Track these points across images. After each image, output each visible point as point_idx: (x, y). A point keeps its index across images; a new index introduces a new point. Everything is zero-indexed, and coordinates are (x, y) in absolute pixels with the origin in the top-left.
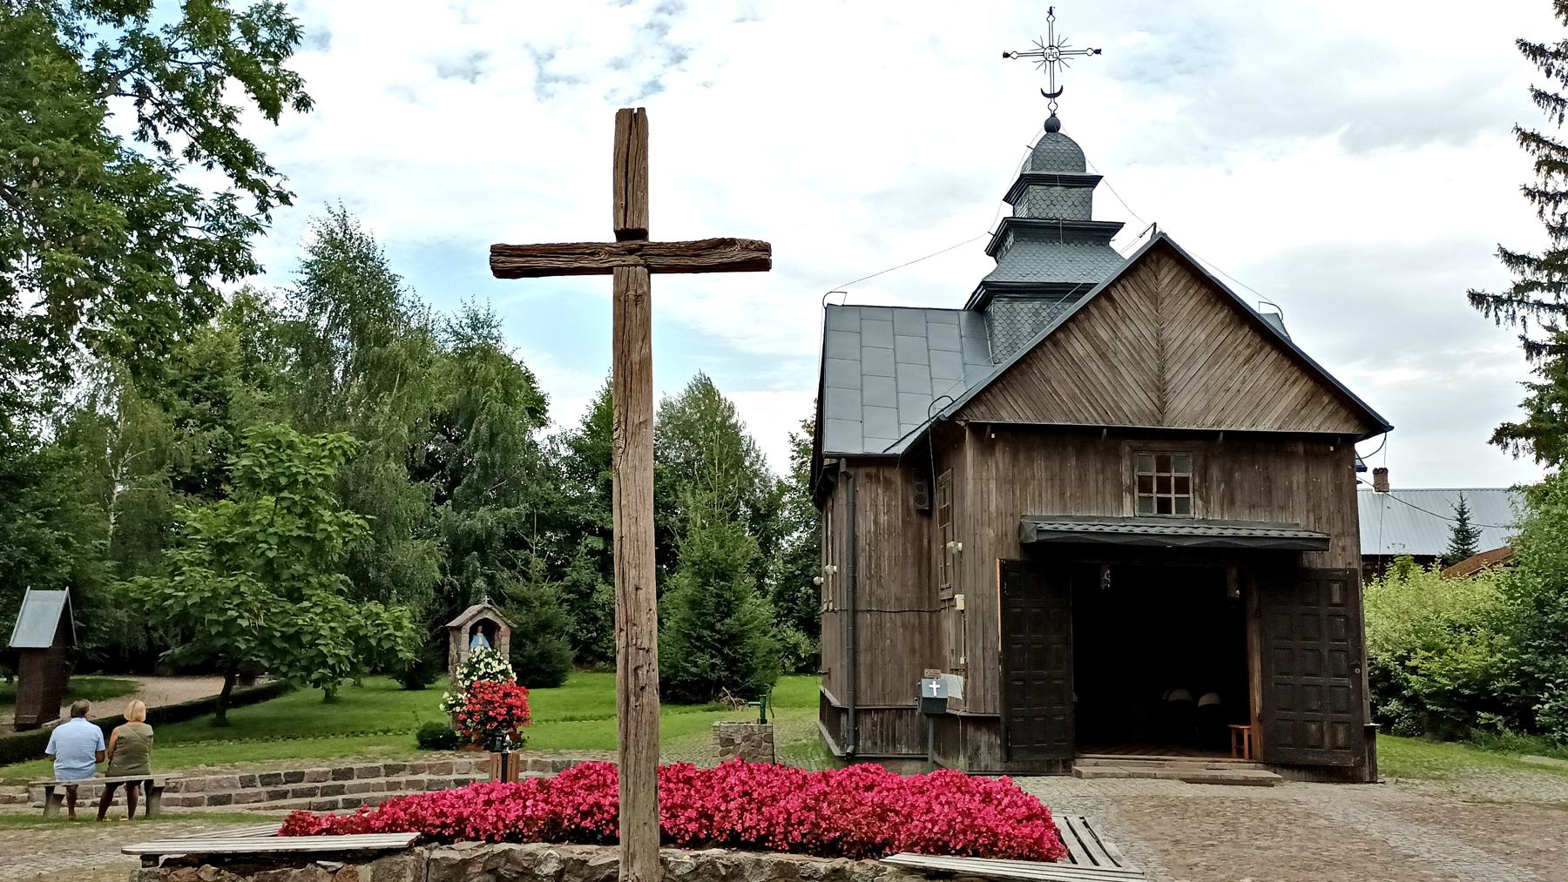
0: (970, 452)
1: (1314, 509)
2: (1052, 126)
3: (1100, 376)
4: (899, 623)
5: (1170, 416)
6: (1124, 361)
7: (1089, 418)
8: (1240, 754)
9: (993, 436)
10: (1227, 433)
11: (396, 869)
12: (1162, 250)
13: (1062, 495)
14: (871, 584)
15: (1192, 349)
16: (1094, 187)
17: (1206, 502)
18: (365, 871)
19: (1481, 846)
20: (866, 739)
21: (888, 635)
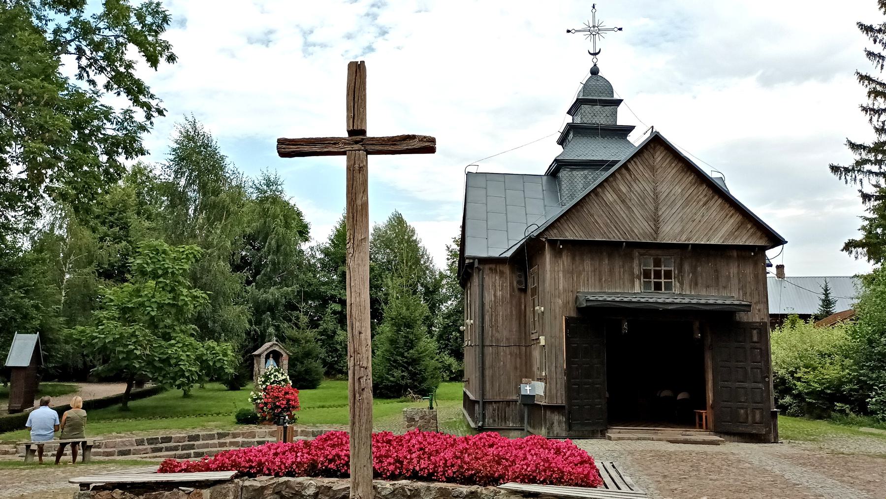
0: (548, 256)
1: (742, 288)
2: (595, 71)
3: (622, 213)
5: (661, 235)
6: (635, 204)
7: (615, 237)
8: (701, 426)
9: (561, 247)
10: (694, 245)
11: (224, 491)
12: (657, 142)
13: (600, 280)
14: (492, 330)
15: (674, 198)
16: (618, 106)
17: (682, 284)
18: (206, 493)
20: (489, 418)
21: (502, 360)
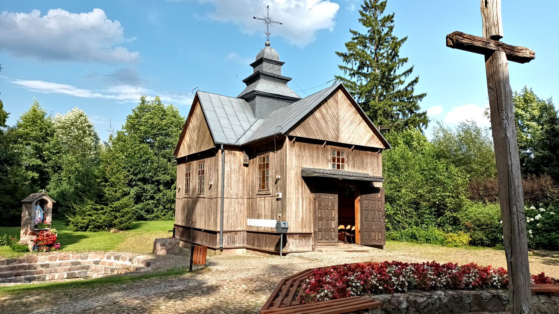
1: (373, 170)
3: (323, 124)
4: (237, 202)
5: (340, 139)
6: (329, 120)
8: (354, 242)
13: (313, 161)
15: (346, 119)
17: (348, 166)
19: (526, 272)
20: (225, 242)
21: (233, 206)
